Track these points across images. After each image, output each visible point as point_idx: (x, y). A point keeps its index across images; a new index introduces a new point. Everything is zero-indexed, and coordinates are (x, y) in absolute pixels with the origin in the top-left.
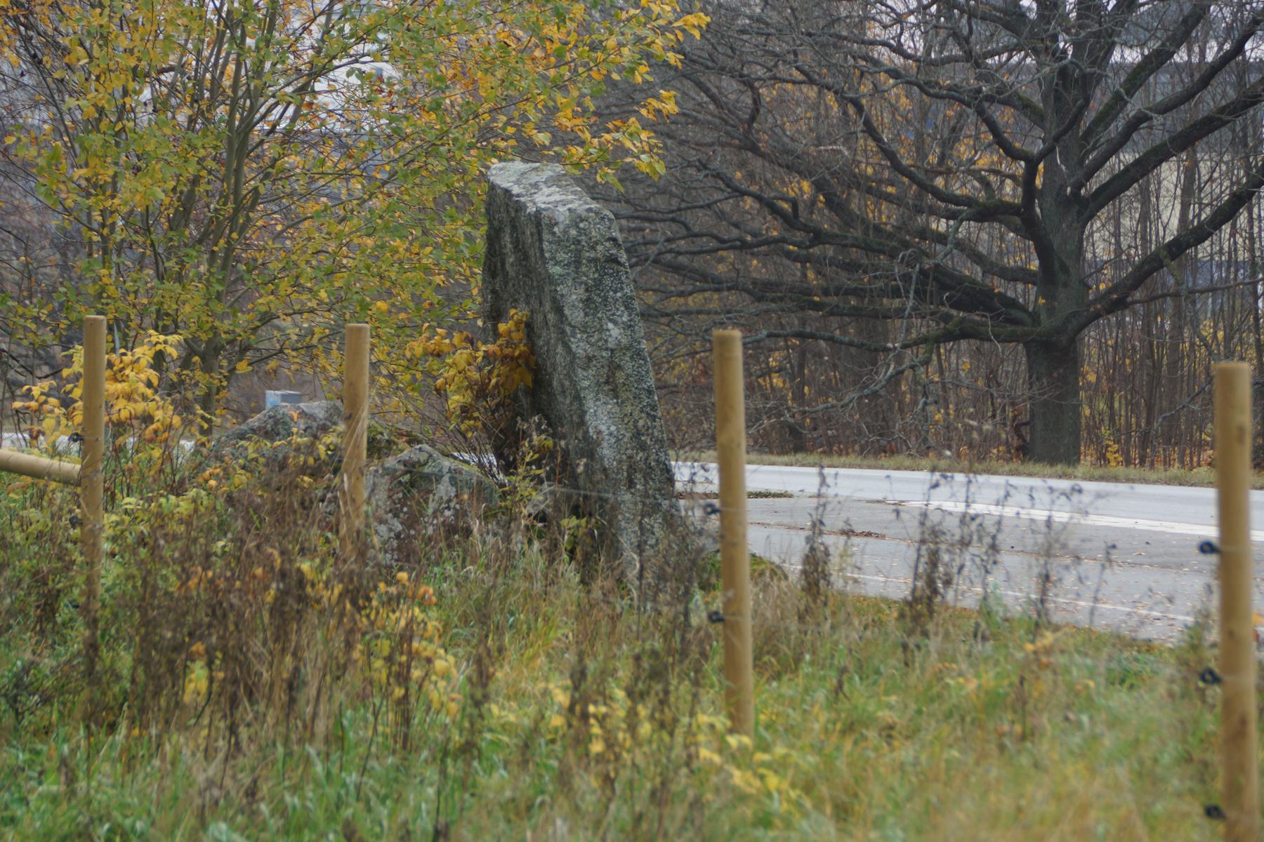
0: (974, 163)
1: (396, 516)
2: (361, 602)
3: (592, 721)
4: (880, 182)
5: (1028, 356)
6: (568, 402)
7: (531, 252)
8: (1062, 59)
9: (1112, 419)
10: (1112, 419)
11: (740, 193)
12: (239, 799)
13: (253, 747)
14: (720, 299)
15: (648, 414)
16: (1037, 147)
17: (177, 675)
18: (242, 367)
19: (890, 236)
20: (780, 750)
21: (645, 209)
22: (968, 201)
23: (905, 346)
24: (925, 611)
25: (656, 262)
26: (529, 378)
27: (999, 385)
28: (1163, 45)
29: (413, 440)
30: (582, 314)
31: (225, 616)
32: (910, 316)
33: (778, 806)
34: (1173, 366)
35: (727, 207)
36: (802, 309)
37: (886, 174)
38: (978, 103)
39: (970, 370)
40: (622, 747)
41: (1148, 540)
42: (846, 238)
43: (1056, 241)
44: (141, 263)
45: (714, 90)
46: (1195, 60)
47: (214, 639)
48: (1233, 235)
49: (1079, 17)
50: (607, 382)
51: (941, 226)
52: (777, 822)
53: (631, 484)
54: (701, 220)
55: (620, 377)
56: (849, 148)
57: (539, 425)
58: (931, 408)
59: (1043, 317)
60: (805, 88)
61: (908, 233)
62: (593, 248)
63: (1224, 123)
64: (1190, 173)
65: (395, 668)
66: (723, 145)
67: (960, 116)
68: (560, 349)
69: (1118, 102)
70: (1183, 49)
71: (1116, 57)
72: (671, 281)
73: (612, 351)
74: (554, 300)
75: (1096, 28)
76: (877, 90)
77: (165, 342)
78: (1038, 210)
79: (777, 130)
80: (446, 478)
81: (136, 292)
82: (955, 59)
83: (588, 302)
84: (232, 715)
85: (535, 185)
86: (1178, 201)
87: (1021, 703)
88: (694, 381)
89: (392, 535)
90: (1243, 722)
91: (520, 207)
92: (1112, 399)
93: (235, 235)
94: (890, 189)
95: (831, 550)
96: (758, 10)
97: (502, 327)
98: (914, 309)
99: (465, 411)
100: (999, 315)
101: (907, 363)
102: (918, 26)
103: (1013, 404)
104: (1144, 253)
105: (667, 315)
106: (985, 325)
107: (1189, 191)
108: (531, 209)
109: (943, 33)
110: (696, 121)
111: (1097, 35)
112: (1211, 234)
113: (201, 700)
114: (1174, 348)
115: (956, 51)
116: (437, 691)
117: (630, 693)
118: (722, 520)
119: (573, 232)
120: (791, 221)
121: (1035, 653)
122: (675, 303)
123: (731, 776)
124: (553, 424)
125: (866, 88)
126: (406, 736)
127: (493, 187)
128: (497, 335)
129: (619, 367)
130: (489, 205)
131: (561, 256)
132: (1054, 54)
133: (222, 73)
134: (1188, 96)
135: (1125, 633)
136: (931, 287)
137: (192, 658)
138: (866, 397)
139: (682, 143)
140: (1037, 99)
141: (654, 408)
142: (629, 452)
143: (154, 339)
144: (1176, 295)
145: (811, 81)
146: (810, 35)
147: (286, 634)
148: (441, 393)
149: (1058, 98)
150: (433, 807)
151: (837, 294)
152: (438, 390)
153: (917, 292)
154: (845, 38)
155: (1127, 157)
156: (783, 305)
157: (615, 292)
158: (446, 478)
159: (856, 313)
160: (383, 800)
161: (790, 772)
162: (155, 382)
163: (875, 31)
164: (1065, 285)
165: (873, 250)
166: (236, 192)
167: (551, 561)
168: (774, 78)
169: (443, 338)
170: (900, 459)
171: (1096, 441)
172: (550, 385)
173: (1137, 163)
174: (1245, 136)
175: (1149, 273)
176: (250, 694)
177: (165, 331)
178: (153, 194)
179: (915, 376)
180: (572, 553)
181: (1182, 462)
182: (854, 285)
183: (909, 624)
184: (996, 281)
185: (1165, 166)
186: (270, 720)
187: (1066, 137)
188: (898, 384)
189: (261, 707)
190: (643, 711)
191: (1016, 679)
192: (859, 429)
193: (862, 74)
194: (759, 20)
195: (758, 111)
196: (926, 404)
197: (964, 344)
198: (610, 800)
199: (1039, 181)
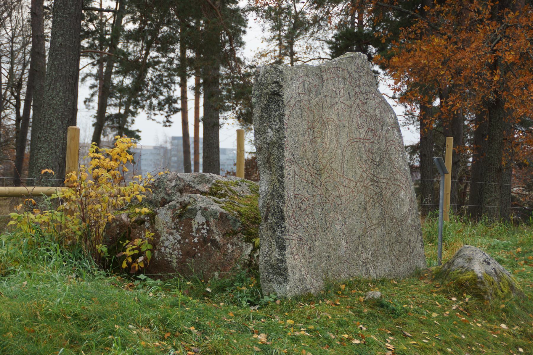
1: (178, 231)
30: (259, 124)
73: (268, 144)
80: (199, 212)
89: (176, 241)
130: (338, 56)
158: (199, 212)
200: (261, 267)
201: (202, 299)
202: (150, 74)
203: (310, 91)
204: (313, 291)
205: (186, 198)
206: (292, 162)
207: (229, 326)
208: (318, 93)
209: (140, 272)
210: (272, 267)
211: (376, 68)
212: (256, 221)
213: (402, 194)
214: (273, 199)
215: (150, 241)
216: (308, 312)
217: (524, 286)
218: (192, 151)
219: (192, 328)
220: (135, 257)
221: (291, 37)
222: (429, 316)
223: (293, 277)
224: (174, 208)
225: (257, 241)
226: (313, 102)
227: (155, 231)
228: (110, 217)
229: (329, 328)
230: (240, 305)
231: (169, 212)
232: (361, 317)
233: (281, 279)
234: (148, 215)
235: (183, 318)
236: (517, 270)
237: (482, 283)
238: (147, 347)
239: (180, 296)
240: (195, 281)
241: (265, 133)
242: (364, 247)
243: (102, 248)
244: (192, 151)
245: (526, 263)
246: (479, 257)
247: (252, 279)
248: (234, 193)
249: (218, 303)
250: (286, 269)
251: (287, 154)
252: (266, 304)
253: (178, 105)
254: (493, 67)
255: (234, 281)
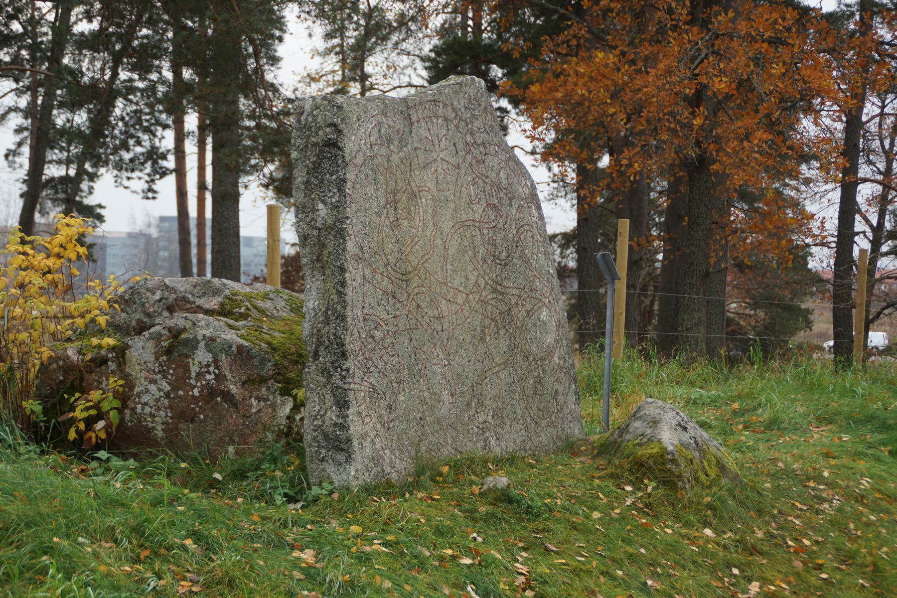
1: (165, 377)
30: (303, 195)
50: (318, 260)
73: (319, 229)
80: (202, 345)
89: (162, 394)
158: (202, 345)
200: (308, 438)
201: (206, 492)
202: (120, 107)
203: (389, 141)
204: (394, 477)
205: (179, 320)
206: (359, 259)
207: (251, 538)
208: (402, 144)
209: (99, 447)
210: (326, 436)
211: (504, 103)
212: (299, 360)
213: (544, 314)
214: (327, 322)
215: (116, 395)
216: (386, 513)
217: (742, 467)
218: (194, 241)
219: (188, 542)
220: (90, 422)
221: (361, 51)
222: (588, 517)
223: (362, 453)
224: (158, 337)
225: (301, 393)
226: (395, 158)
227: (126, 376)
228: (46, 353)
229: (421, 539)
230: (270, 502)
231: (150, 345)
232: (475, 520)
233: (341, 457)
234: (113, 349)
235: (172, 524)
236: (731, 440)
237: (673, 461)
238: (109, 575)
239: (167, 487)
240: (194, 461)
241: (314, 210)
242: (480, 403)
243: (32, 406)
244: (194, 241)
245: (746, 427)
246: (670, 418)
247: (292, 457)
248: (262, 312)
249: (234, 498)
250: (349, 440)
251: (351, 246)
252: (316, 500)
253: (170, 163)
254: (696, 100)
255: (261, 461)
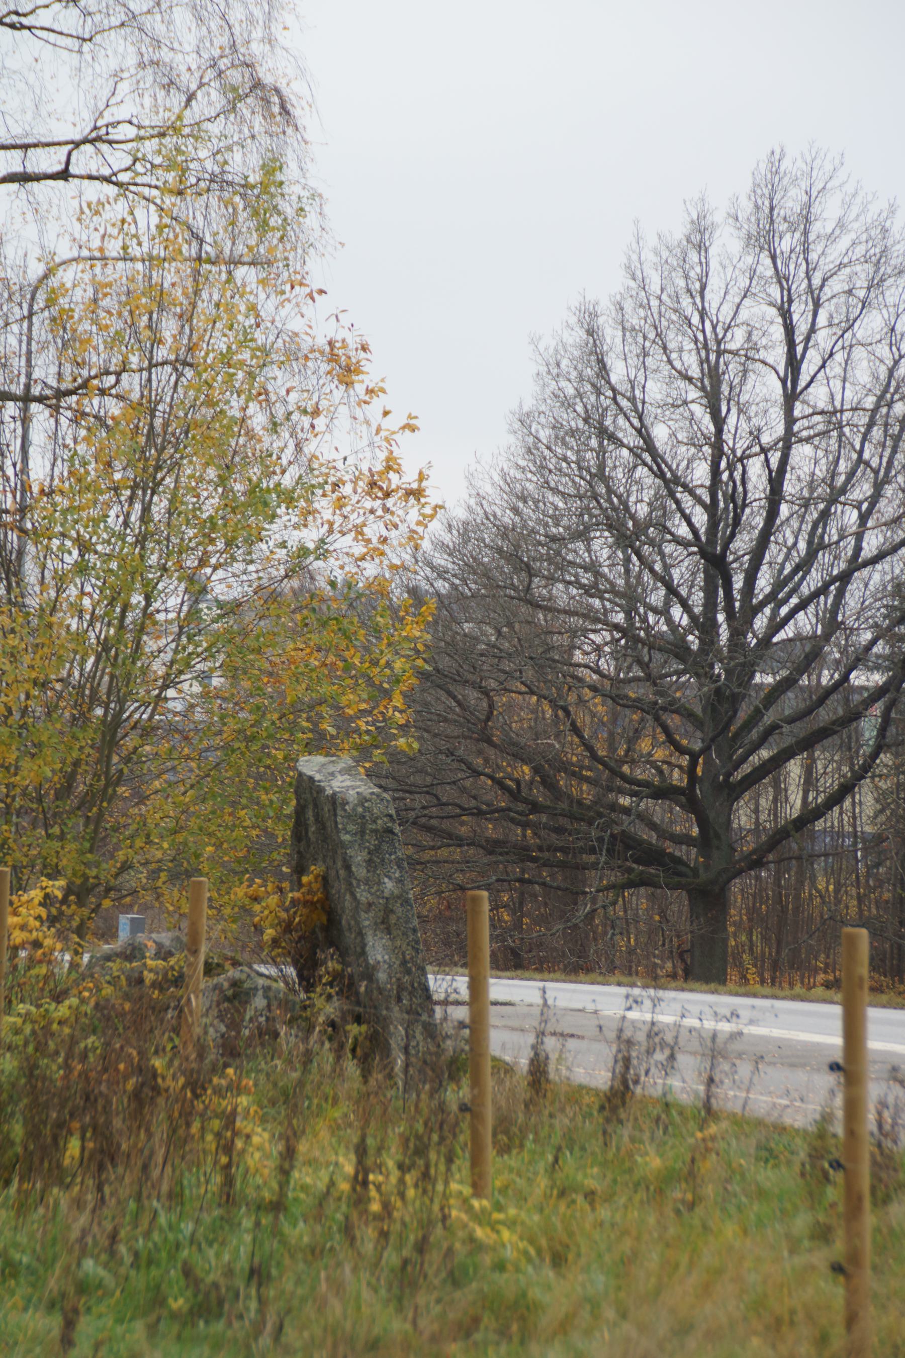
0: (652, 756)
1: (222, 1021)
2: (199, 1091)
3: (371, 1187)
4: (582, 768)
5: (690, 901)
6: (353, 936)
7: (328, 824)
8: (717, 681)
9: (751, 949)
10: (751, 949)
11: (477, 773)
12: (104, 1242)
13: (113, 1200)
14: (461, 852)
15: (413, 947)
16: (697, 746)
17: (57, 1144)
18: (107, 903)
19: (589, 808)
20: (512, 1211)
21: (407, 784)
22: (647, 784)
23: (598, 891)
24: (619, 1102)
25: (414, 823)
26: (324, 919)
27: (668, 921)
28: (791, 673)
29: (236, 963)
30: (365, 871)
31: (96, 1100)
32: (603, 868)
33: (509, 1254)
34: (796, 909)
35: (468, 783)
36: (522, 861)
37: (587, 762)
38: (654, 712)
39: (646, 909)
40: (394, 1208)
41: (780, 1045)
42: (556, 809)
43: (712, 815)
44: (34, 825)
45: (460, 697)
46: (814, 682)
47: (88, 1119)
48: (841, 814)
49: (729, 651)
50: (383, 923)
51: (625, 801)
52: (509, 1267)
53: (399, 999)
54: (447, 793)
55: (393, 919)
56: (559, 742)
57: (332, 956)
58: (617, 937)
59: (701, 871)
60: (527, 697)
61: (602, 806)
62: (375, 822)
63: (835, 732)
64: (809, 770)
65: (222, 1142)
66: (465, 738)
67: (642, 719)
68: (348, 897)
69: (757, 714)
70: (805, 677)
71: (758, 678)
72: (426, 839)
74: (344, 860)
75: (742, 660)
76: (581, 701)
77: (53, 886)
78: (698, 792)
79: (507, 728)
81: (29, 846)
82: (636, 679)
83: (369, 862)
84: (99, 1176)
85: (332, 774)
86: (801, 788)
87: (691, 1176)
88: (440, 913)
90: (860, 1199)
91: (321, 790)
92: (750, 934)
93: (105, 804)
94: (589, 773)
95: (551, 1056)
96: (493, 638)
97: (305, 879)
98: (606, 863)
99: (275, 942)
100: (669, 869)
101: (599, 904)
102: (611, 653)
103: (678, 936)
104: (776, 826)
105: (422, 863)
106: (658, 876)
107: (809, 782)
108: (329, 792)
109: (629, 660)
110: (446, 720)
111: (743, 665)
112: (824, 814)
113: (76, 1162)
114: (797, 897)
115: (639, 673)
116: (253, 1159)
117: (401, 1166)
118: (471, 1031)
119: (360, 810)
120: (515, 795)
121: (704, 1140)
122: (428, 855)
123: (474, 1231)
124: (343, 955)
125: (572, 698)
126: (228, 1195)
127: (301, 774)
128: (300, 885)
129: (392, 911)
131: (351, 827)
132: (711, 678)
133: (99, 684)
134: (809, 711)
135: (769, 1120)
136: (619, 847)
137: (70, 1133)
138: (569, 928)
139: (436, 735)
140: (698, 710)
141: (417, 942)
142: (398, 975)
143: (44, 884)
144: (799, 858)
145: (532, 693)
146: (531, 658)
147: (141, 1113)
148: (259, 929)
149: (714, 710)
150: (250, 1248)
151: (548, 851)
152: (255, 926)
153: (608, 850)
154: (558, 661)
155: (765, 754)
156: (507, 857)
157: (390, 855)
158: (260, 993)
159: (563, 865)
160: (210, 1244)
161: (519, 1228)
162: (44, 916)
163: (578, 657)
164: (718, 848)
165: (576, 819)
166: (107, 773)
167: (338, 1058)
168: (505, 689)
169: (260, 886)
170: (593, 976)
171: (739, 965)
172: (340, 923)
173: (772, 759)
174: (850, 742)
175: (779, 842)
176: (112, 1159)
177: (50, 877)
178: (43, 772)
179: (605, 913)
180: (353, 1051)
181: (802, 983)
182: (561, 844)
183: (606, 1113)
184: (668, 843)
185: (792, 761)
186: (127, 1180)
187: (720, 738)
188: (593, 918)
189: (120, 1170)
190: (409, 1179)
191: (688, 1159)
192: (563, 952)
193: (570, 689)
194: (494, 646)
195: (492, 713)
196: (613, 934)
197: (642, 890)
198: (384, 1248)
199: (699, 771)
